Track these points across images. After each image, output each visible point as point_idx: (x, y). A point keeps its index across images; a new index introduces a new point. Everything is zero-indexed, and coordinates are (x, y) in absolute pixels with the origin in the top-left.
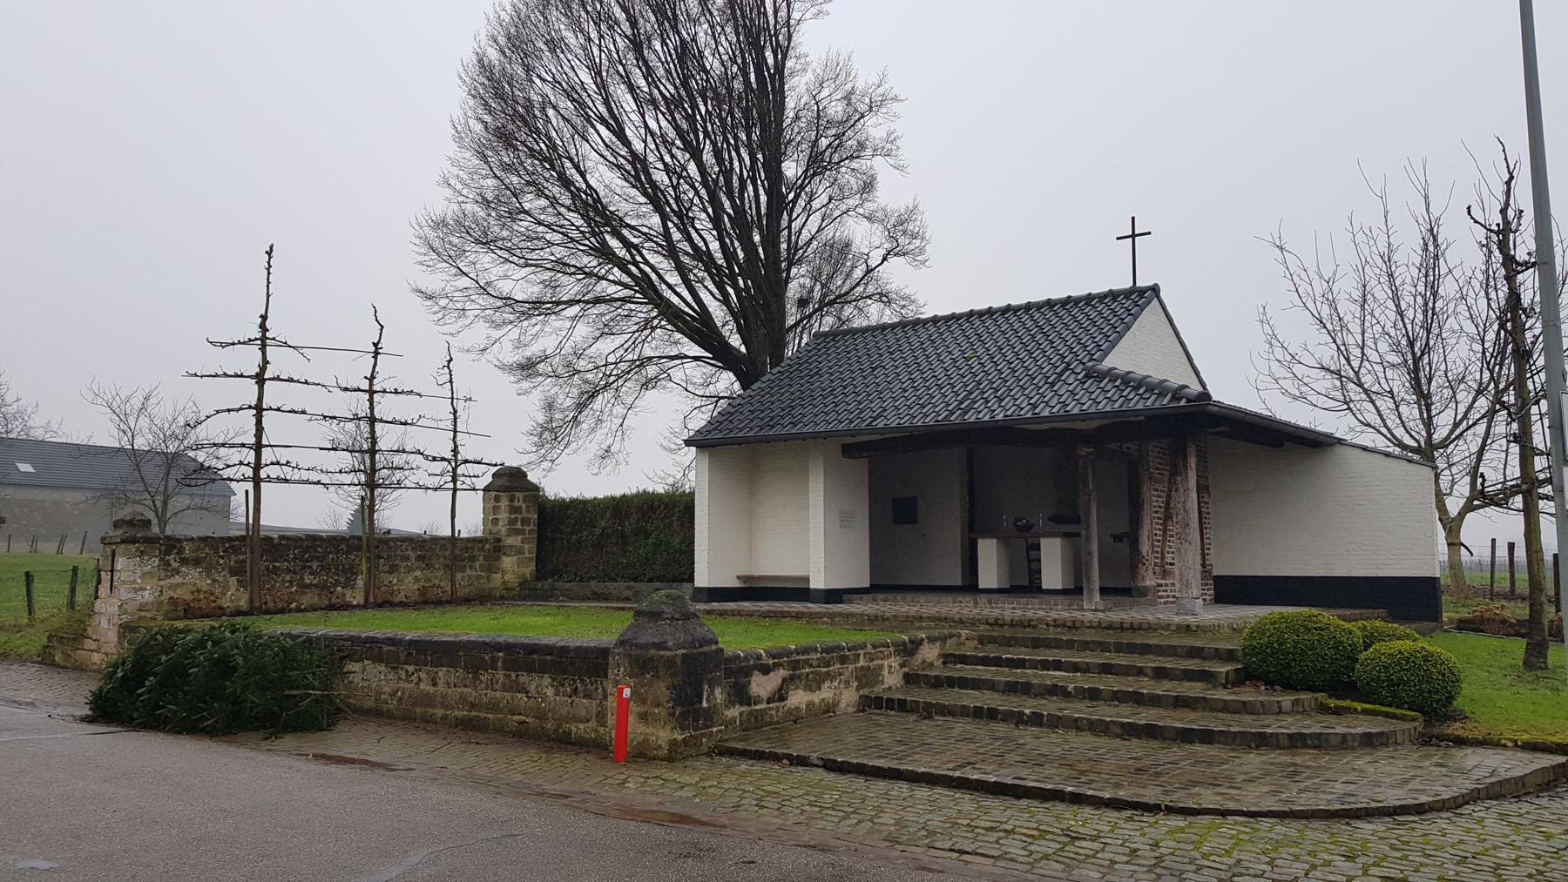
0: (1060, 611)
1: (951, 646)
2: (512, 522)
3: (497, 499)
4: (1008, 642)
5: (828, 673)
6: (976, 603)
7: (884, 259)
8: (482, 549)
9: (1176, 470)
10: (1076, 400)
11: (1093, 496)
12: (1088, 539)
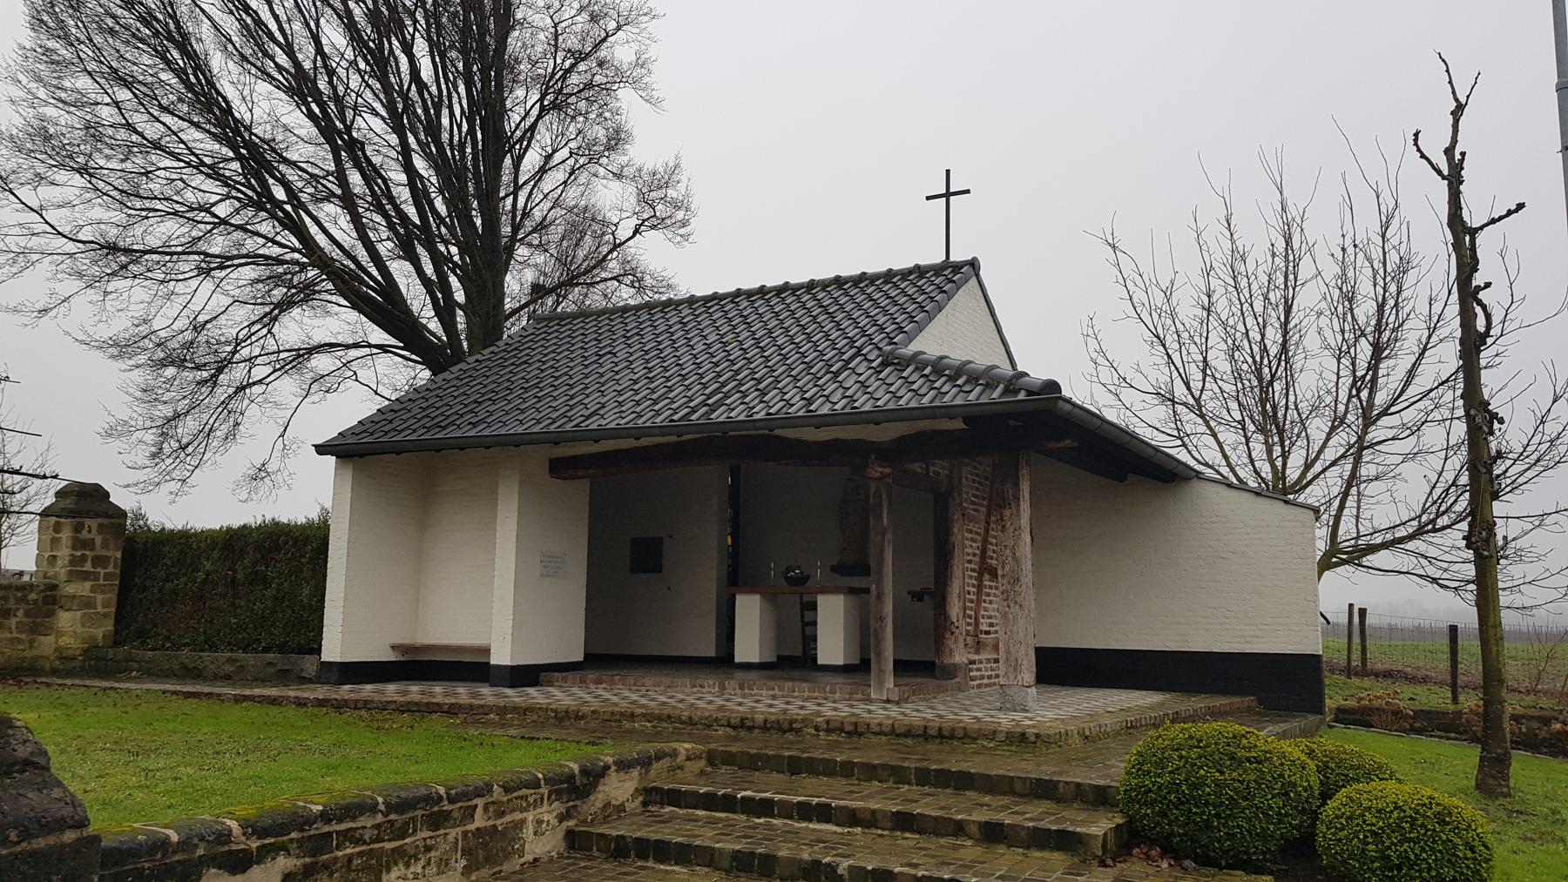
0: (835, 706)
1: (658, 776)
2: (74, 561)
3: (57, 528)
4: (753, 763)
5: (399, 853)
6: (722, 688)
7: (636, 231)
8: (24, 600)
9: (999, 503)
10: (870, 392)
11: (889, 536)
12: (879, 597)
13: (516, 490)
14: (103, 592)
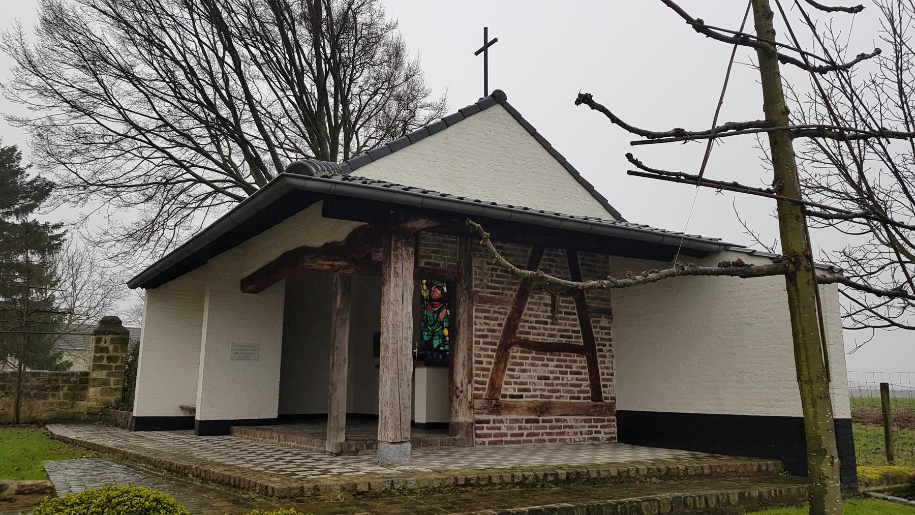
14: (114, 376)
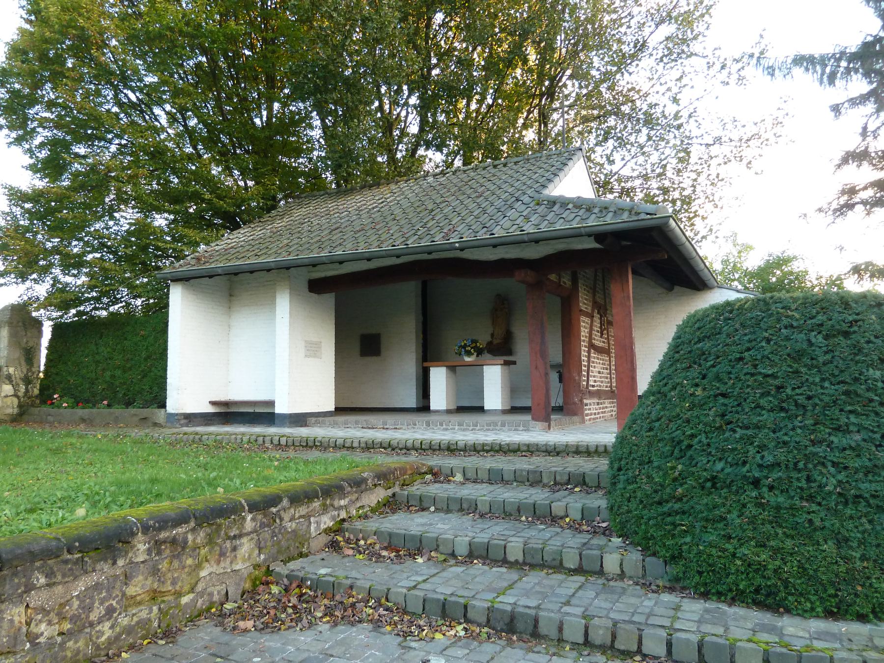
13: (288, 295)
